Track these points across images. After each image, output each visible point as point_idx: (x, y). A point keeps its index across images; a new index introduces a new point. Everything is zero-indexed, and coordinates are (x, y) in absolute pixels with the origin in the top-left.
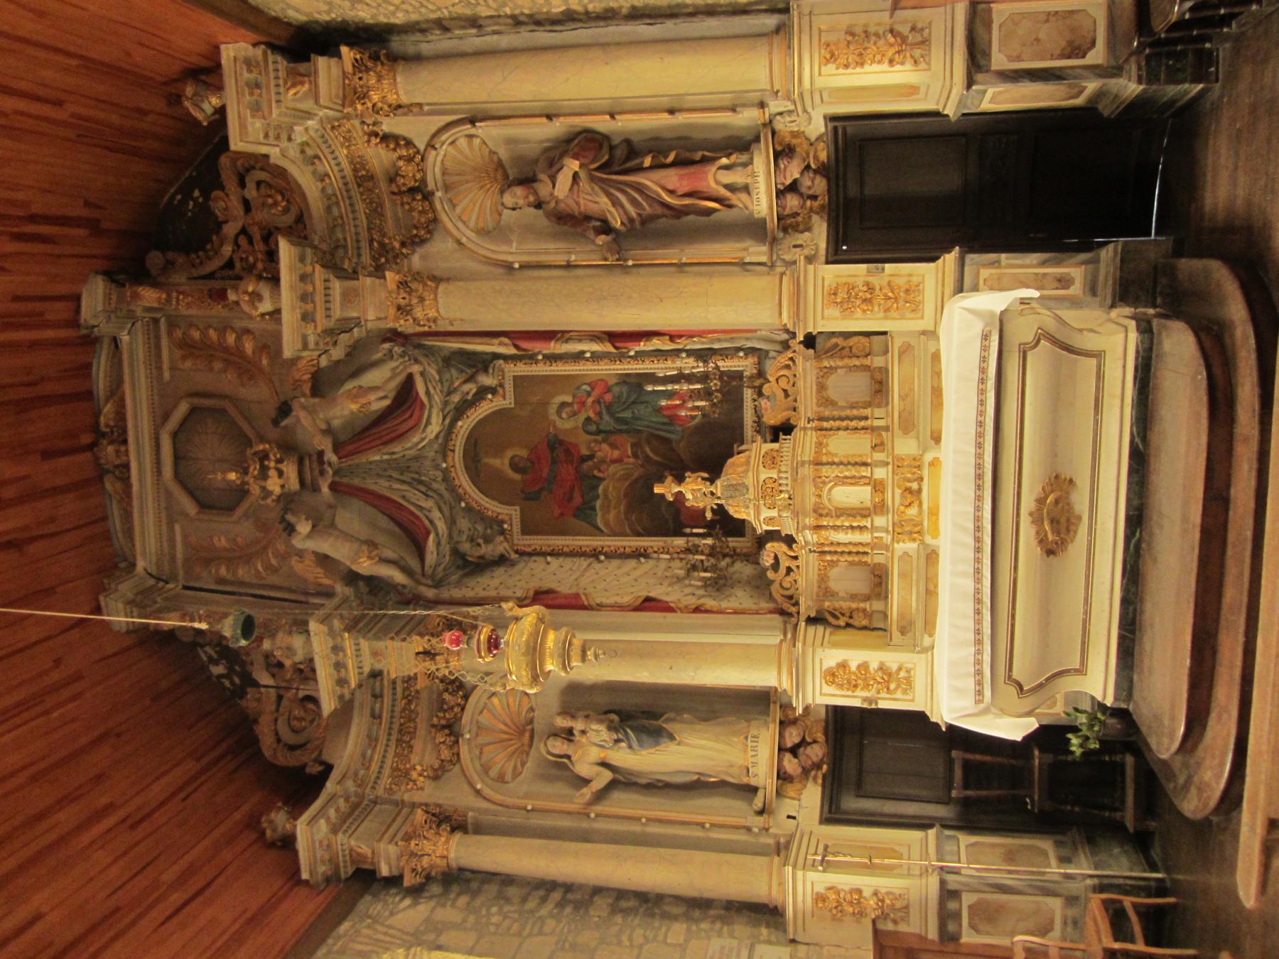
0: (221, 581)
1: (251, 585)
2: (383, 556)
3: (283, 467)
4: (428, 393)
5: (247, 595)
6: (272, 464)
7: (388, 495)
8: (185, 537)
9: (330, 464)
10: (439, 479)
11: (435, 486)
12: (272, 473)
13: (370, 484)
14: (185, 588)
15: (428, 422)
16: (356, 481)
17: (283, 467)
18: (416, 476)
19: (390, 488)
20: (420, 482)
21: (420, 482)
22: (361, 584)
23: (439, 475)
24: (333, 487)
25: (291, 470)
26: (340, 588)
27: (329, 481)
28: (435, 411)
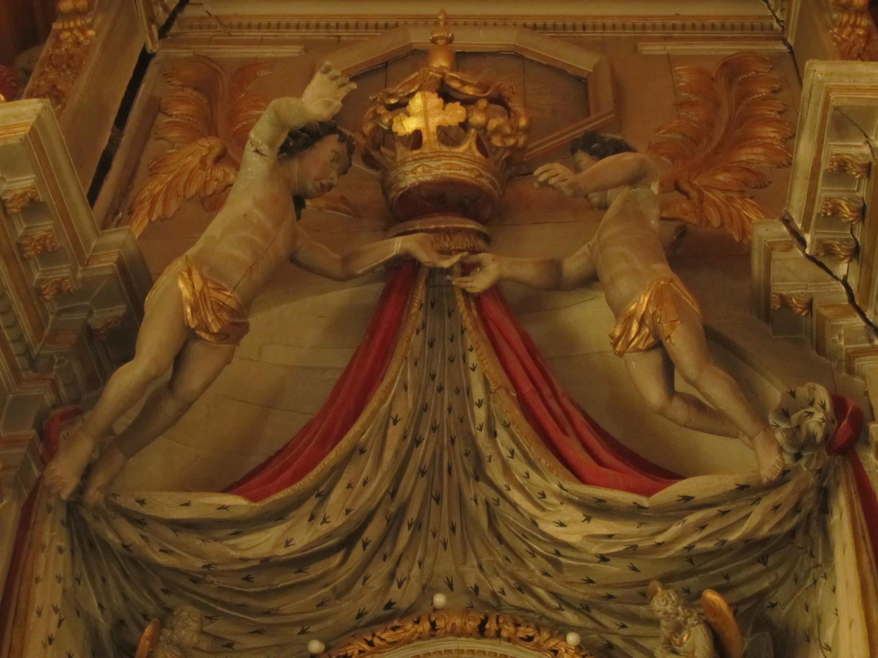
0: (155, 108)
1: (139, 147)
2: (196, 348)
3: (468, 146)
4: (688, 505)
5: (114, 143)
6: (478, 119)
7: (373, 404)
8: (271, 63)
9: (467, 269)
10: (395, 593)
11: (379, 570)
12: (455, 114)
13: (399, 372)
14: (145, 58)
15: (596, 509)
16: (411, 340)
17: (468, 146)
18: (412, 514)
19: (391, 419)
20: (394, 523)
21: (394, 523)
22: (120, 310)
23: (403, 596)
24: (402, 272)
25: (460, 164)
26: (121, 239)
27: (424, 256)
28: (628, 530)
